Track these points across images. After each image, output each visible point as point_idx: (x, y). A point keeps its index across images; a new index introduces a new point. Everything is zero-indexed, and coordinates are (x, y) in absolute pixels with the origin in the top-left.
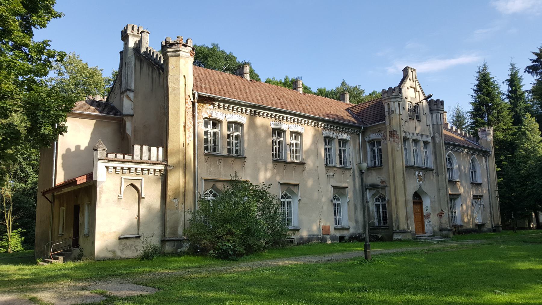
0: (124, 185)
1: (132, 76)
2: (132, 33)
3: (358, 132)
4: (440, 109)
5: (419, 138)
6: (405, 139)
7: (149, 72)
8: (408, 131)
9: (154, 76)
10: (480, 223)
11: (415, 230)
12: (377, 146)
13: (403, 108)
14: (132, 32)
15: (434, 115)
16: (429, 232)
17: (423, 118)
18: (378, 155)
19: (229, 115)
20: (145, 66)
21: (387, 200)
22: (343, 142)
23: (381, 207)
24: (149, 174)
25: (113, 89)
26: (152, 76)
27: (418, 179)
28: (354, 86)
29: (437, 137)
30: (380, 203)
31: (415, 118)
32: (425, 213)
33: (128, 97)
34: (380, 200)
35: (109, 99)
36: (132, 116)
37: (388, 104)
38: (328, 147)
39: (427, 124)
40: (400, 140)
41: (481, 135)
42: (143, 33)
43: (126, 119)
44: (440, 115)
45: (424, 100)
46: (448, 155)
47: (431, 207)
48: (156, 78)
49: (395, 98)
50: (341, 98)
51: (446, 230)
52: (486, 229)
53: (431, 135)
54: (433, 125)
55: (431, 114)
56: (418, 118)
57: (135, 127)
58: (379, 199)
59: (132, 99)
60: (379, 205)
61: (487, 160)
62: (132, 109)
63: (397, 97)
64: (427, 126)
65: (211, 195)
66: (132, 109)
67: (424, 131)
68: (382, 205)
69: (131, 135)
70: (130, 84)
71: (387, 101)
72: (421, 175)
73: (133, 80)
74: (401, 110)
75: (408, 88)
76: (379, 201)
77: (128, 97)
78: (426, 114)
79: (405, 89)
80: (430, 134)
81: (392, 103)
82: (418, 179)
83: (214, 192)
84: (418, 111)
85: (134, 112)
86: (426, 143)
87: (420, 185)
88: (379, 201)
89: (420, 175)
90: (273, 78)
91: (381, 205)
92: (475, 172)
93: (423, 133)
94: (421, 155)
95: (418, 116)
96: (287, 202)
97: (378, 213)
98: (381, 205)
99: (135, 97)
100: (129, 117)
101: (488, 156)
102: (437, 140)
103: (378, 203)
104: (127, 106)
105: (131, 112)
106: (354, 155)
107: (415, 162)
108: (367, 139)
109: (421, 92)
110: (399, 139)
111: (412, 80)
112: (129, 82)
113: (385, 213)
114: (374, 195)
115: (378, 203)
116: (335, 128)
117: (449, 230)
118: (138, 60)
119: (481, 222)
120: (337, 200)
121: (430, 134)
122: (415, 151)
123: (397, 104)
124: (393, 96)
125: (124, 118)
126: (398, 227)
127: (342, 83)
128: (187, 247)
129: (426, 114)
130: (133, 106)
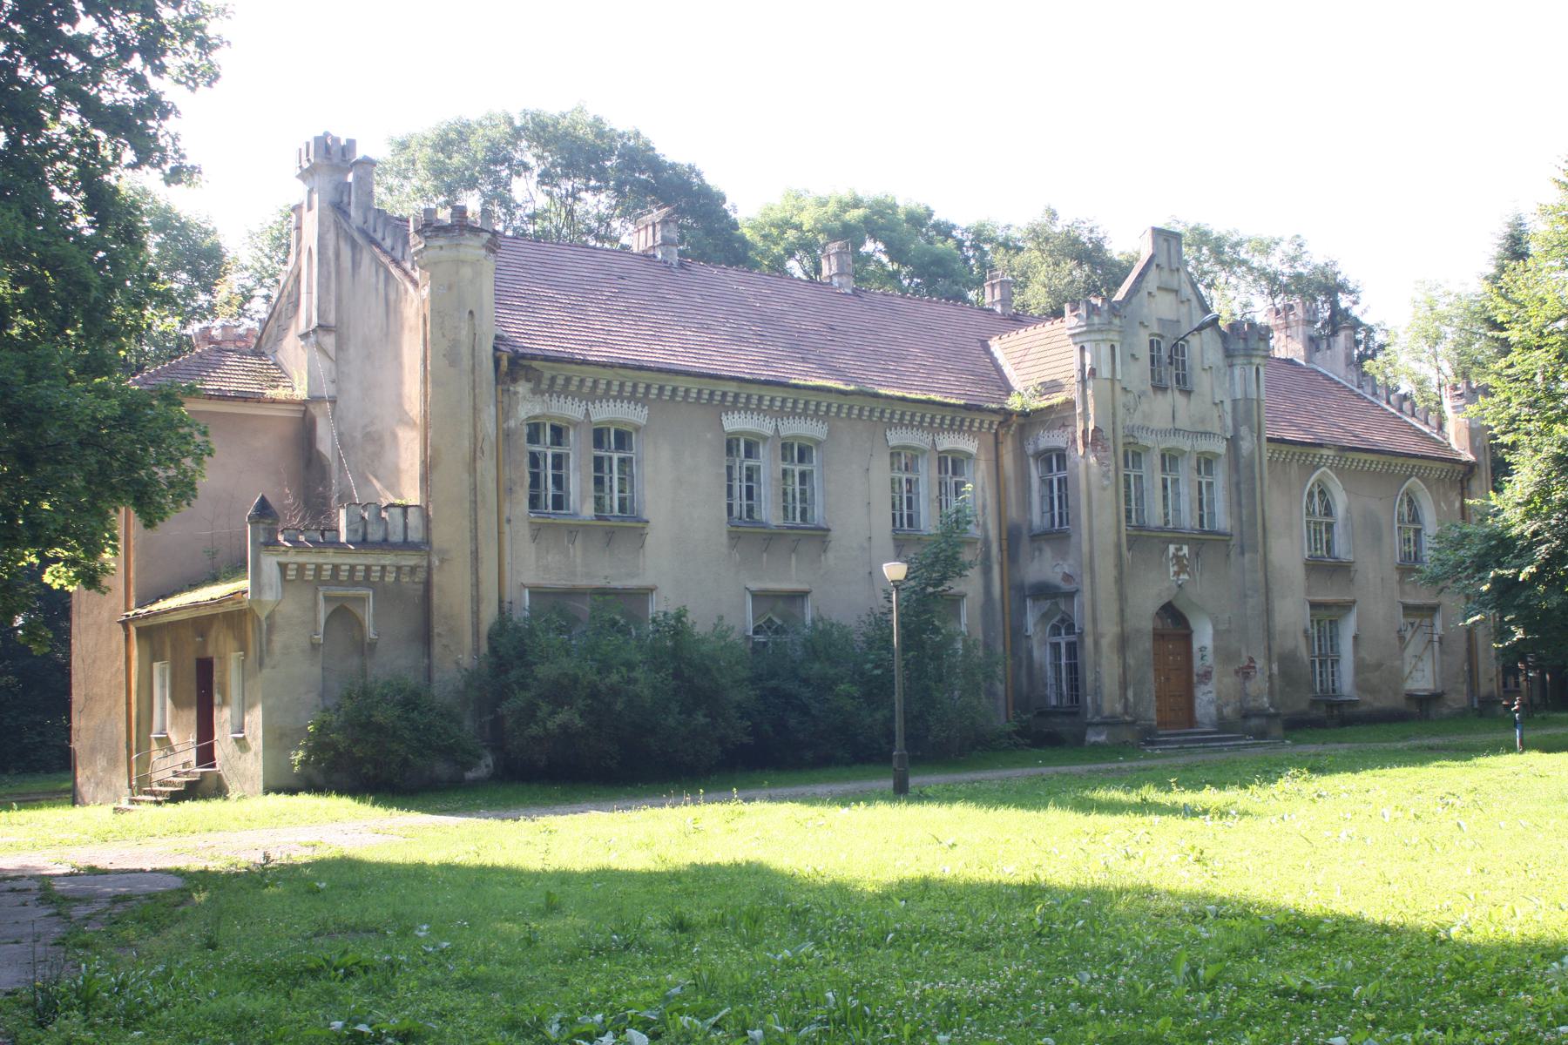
5: (1185, 444)
7: (378, 282)
10: (1425, 690)
11: (1155, 717)
15: (1237, 371)
16: (1207, 721)
17: (1203, 382)
21: (1077, 631)
23: (1063, 650)
27: (1176, 568)
28: (377, 807)
29: (1242, 439)
30: (1063, 640)
32: (1198, 665)
34: (1063, 632)
44: (1257, 370)
47: (1216, 649)
51: (1260, 713)
52: (1445, 711)
54: (1235, 401)
56: (1185, 383)
58: (1059, 629)
59: (332, 353)
60: (1059, 644)
64: (1216, 404)
67: (1202, 421)
68: (1068, 644)
69: (329, 456)
73: (333, 300)
75: (1150, 293)
76: (1060, 634)
80: (1223, 428)
84: (1183, 362)
86: (1206, 462)
87: (1180, 586)
88: (1060, 634)
89: (1181, 553)
93: (1200, 428)
95: (1184, 375)
97: (1057, 668)
102: (1246, 446)
103: (1055, 639)
106: (988, 496)
108: (1030, 449)
110: (1110, 453)
111: (1166, 269)
113: (1074, 669)
114: (1045, 617)
115: (1055, 639)
117: (1270, 717)
119: (1431, 686)
126: (1098, 710)
128: (487, 766)
130: (334, 373)
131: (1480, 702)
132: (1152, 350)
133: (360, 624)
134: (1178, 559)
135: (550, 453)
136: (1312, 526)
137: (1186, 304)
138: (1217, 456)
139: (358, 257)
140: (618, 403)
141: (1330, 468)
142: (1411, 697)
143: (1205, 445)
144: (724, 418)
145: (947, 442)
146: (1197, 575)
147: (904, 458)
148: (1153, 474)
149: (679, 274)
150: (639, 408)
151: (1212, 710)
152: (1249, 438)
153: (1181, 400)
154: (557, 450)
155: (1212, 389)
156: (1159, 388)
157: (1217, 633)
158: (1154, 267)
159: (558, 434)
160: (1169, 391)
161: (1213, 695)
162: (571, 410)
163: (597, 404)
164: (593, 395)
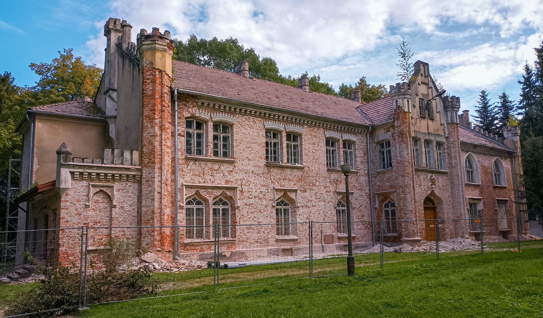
0: (93, 191)
1: (114, 75)
2: (115, 28)
3: (366, 133)
4: (455, 106)
6: (416, 140)
7: (130, 70)
8: (419, 130)
9: (135, 73)
12: (386, 147)
13: (414, 105)
14: (114, 27)
17: (437, 116)
18: (387, 157)
19: (215, 115)
20: (127, 62)
22: (348, 144)
23: (390, 213)
24: (122, 180)
25: (100, 90)
26: (133, 73)
31: (427, 116)
33: (111, 97)
34: (390, 206)
35: (96, 100)
36: (115, 117)
37: (397, 101)
38: (331, 149)
39: (441, 122)
40: (410, 142)
41: (507, 134)
42: (125, 27)
43: (109, 121)
45: (436, 96)
46: (468, 157)
48: (136, 75)
49: (404, 94)
50: (353, 97)
53: (445, 134)
55: (446, 111)
57: (118, 129)
58: (388, 205)
61: (514, 162)
62: (116, 110)
63: (406, 93)
65: (195, 203)
66: (116, 110)
67: (437, 130)
70: (113, 83)
71: (395, 98)
72: (434, 178)
74: (410, 108)
75: (419, 84)
77: (111, 97)
78: (439, 112)
79: (417, 85)
80: (444, 133)
81: (401, 100)
82: (431, 183)
83: (199, 199)
85: (117, 113)
89: (432, 178)
90: (290, 76)
91: (390, 211)
92: (499, 175)
93: (437, 133)
94: (434, 156)
96: (285, 210)
98: (390, 211)
99: (118, 96)
100: (112, 119)
101: (514, 157)
104: (110, 108)
105: (114, 113)
107: (428, 164)
109: (434, 89)
111: (423, 76)
112: (112, 81)
116: (339, 128)
118: (121, 57)
120: (342, 206)
121: (444, 133)
122: (427, 152)
123: (406, 101)
124: (401, 92)
125: (107, 120)
127: (361, 80)
129: (439, 112)
130: (116, 107)
132: (420, 104)
135: (195, 132)
136: (98, 260)
137: (431, 89)
139: (125, 61)
141: (471, 152)
143: (439, 139)
145: (346, 137)
147: (330, 142)
149: (250, 80)
153: (430, 122)
155: (440, 119)
156: (423, 118)
160: (426, 119)
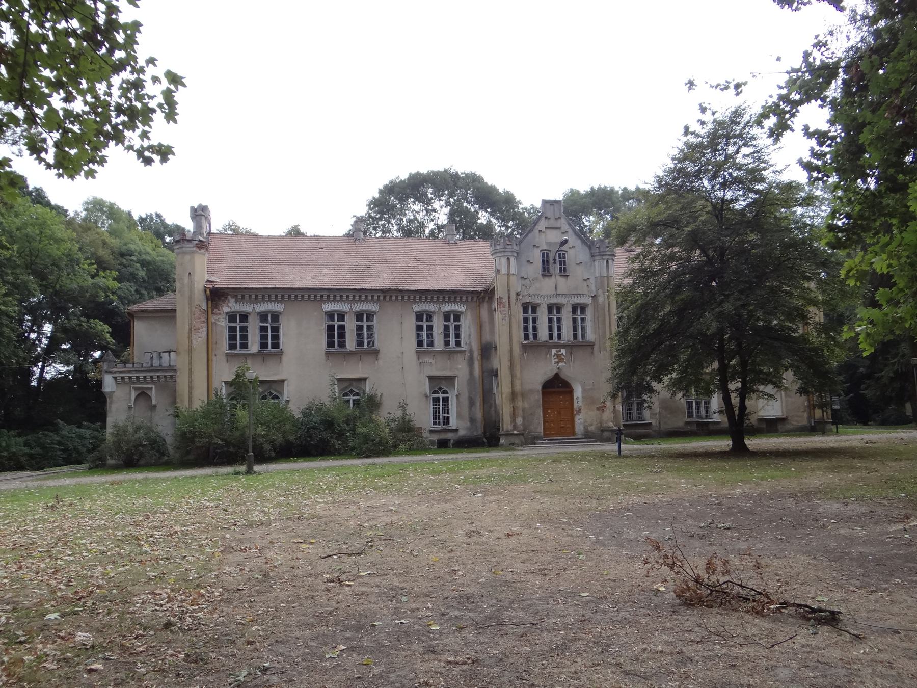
15: (596, 263)
27: (556, 360)
47: (583, 397)
131: (815, 422)
133: (150, 398)
134: (558, 356)
138: (587, 305)
140: (269, 304)
142: (761, 420)
144: (323, 306)
145: (447, 308)
146: (571, 364)
148: (543, 317)
150: (279, 305)
151: (582, 428)
152: (602, 295)
153: (561, 281)
154: (429, 324)
157: (584, 391)
158: (544, 218)
159: (429, 318)
161: (582, 420)
162: (246, 308)
163: (259, 305)
164: (257, 301)
